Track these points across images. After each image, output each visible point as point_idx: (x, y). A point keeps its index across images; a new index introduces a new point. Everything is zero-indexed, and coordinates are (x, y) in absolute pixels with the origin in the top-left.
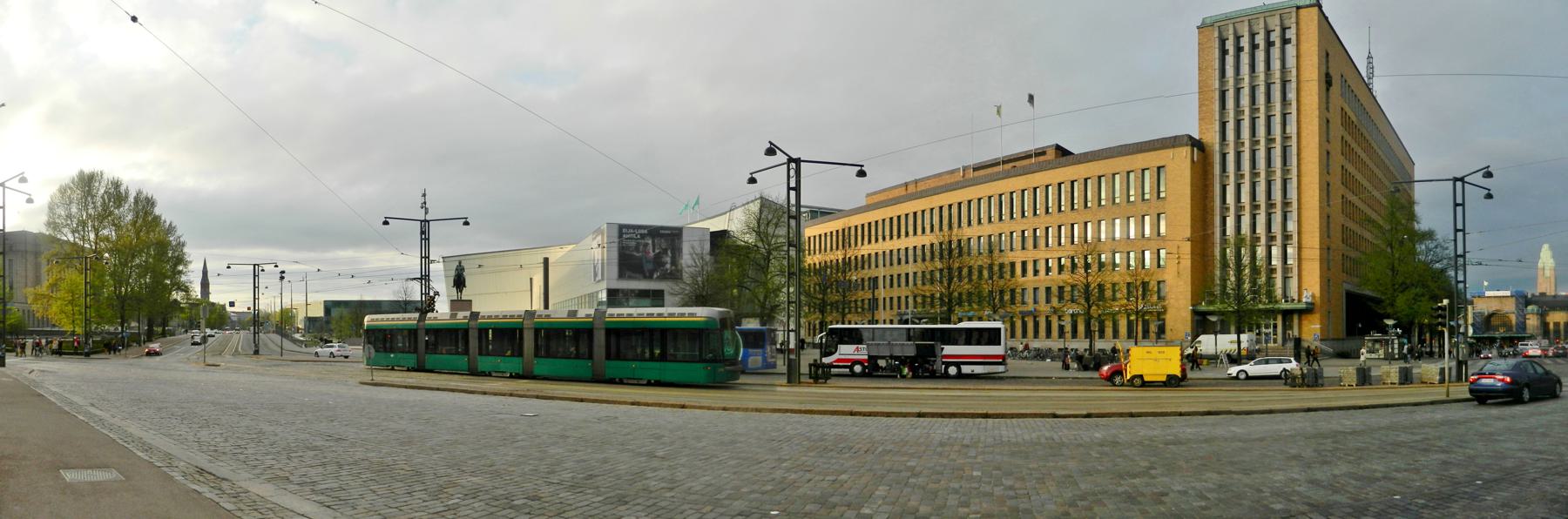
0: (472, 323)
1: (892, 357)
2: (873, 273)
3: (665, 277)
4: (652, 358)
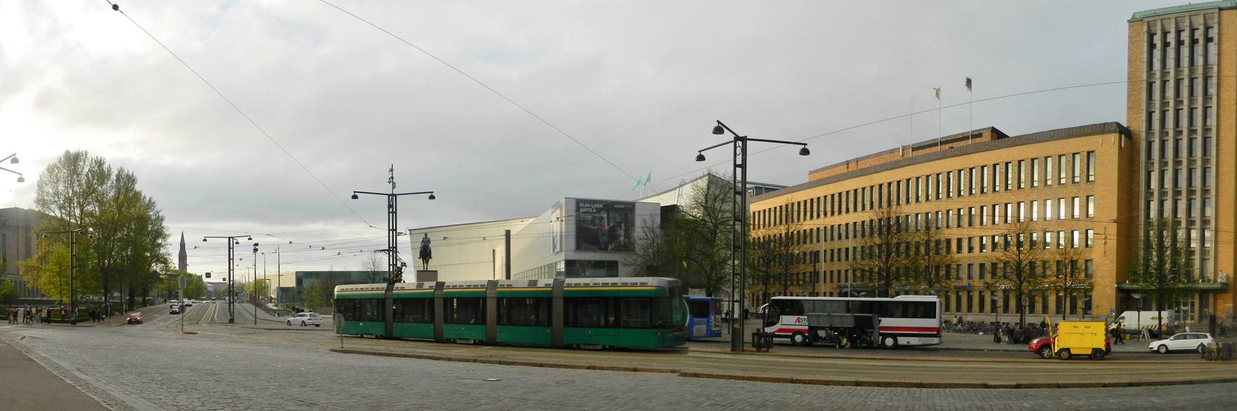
0: (438, 293)
1: (831, 328)
2: (814, 247)
3: (619, 248)
4: (607, 325)
